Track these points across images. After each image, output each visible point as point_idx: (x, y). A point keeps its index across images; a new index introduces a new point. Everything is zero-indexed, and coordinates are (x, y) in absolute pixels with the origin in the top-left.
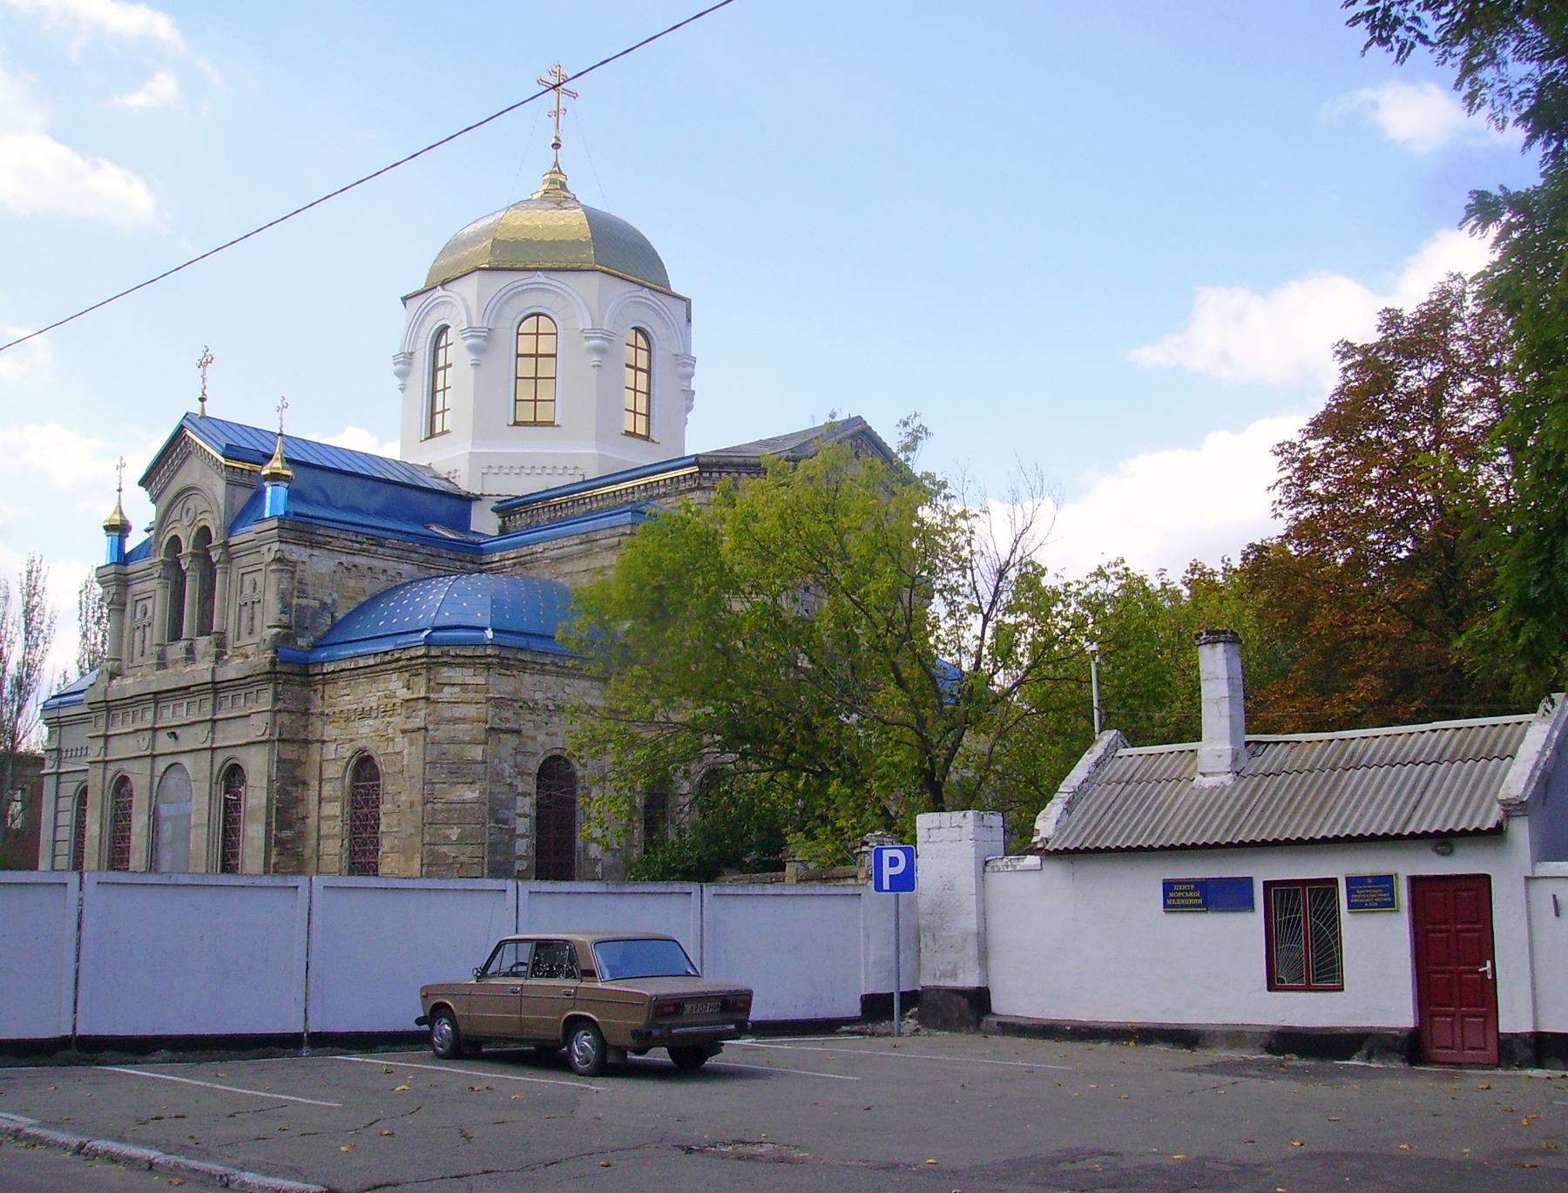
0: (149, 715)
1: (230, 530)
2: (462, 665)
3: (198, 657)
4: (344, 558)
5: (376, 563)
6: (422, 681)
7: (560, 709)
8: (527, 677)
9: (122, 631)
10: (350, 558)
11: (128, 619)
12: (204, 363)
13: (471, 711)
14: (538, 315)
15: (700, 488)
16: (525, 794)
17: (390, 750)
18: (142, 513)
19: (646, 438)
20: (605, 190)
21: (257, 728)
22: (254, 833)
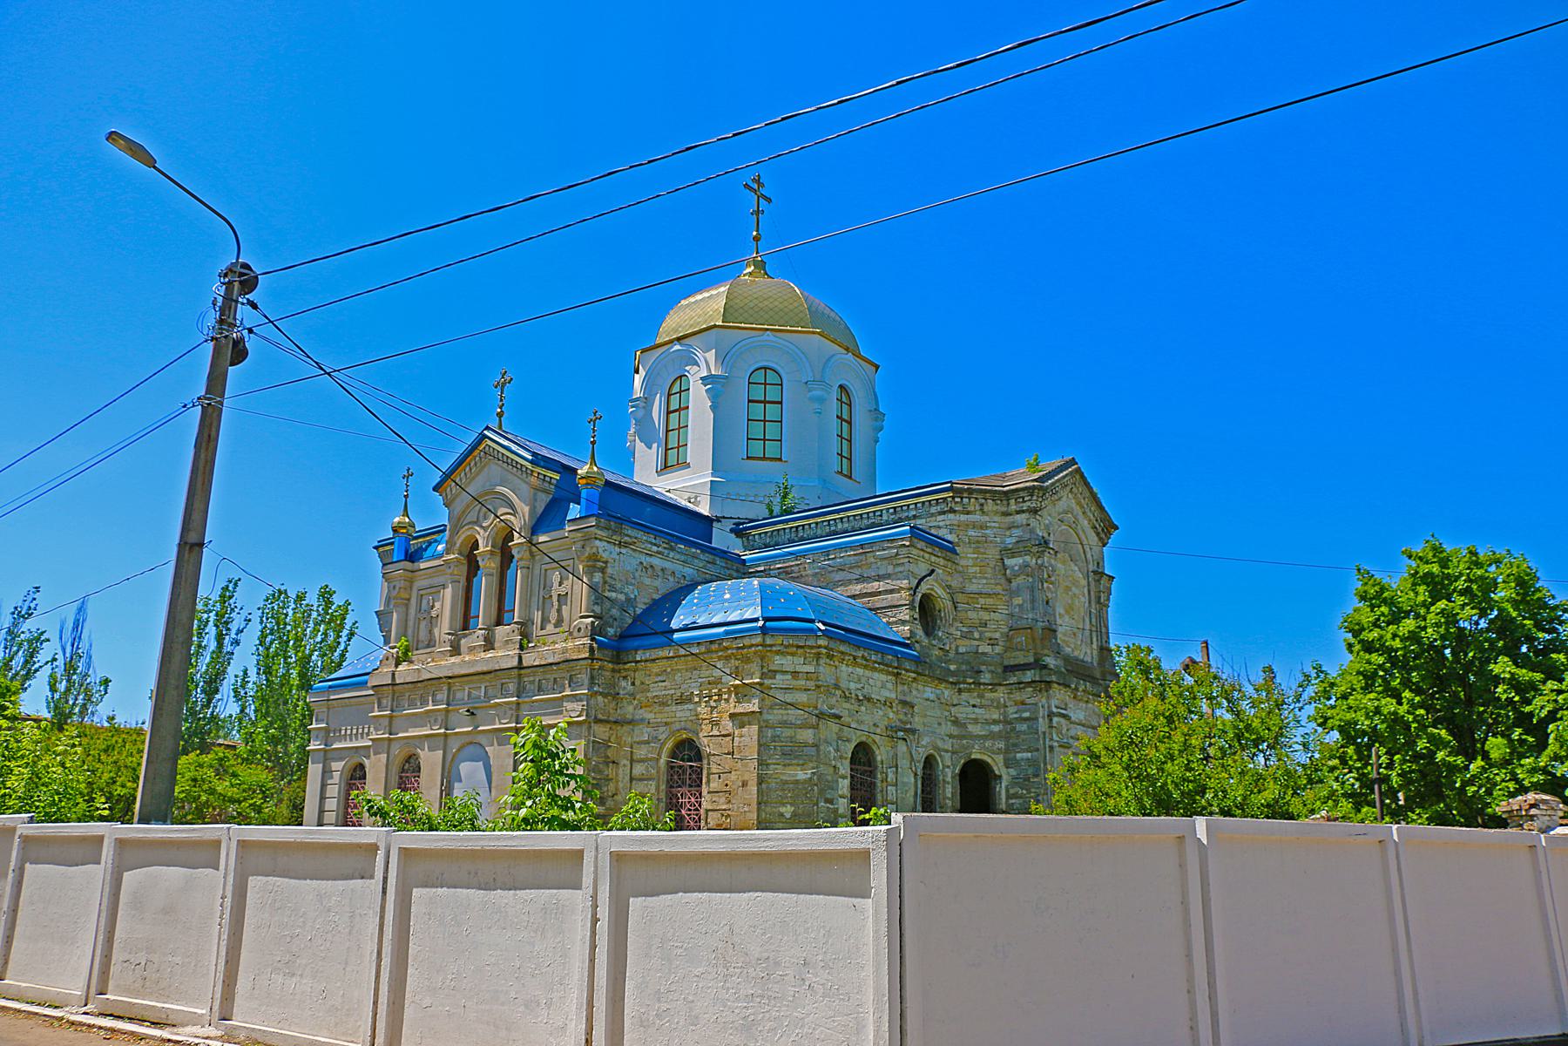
1: (535, 529)
5: (667, 565)
6: (754, 667)
7: (869, 699)
11: (412, 611)
14: (765, 368)
15: (952, 511)
16: (844, 777)
17: (715, 732)
22: (331, 804)
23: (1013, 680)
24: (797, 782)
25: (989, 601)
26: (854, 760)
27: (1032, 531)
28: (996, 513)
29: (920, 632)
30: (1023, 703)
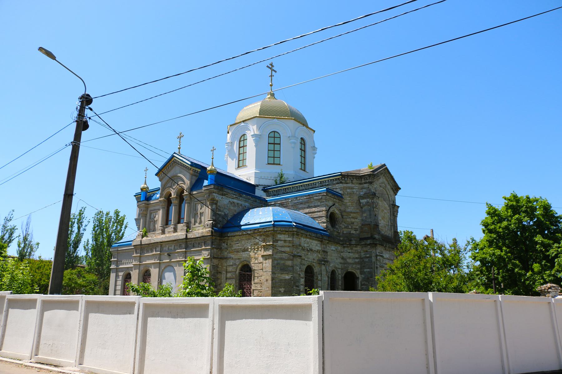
2: (284, 234)
3: (178, 231)
4: (231, 200)
5: (239, 202)
6: (270, 239)
7: (311, 250)
8: (302, 239)
9: (146, 222)
10: (233, 200)
11: (148, 218)
12: (180, 138)
13: (287, 249)
14: (274, 132)
15: (341, 183)
16: (302, 278)
17: (256, 262)
18: (155, 183)
19: (305, 171)
20: (284, 101)
21: (206, 254)
23: (363, 243)
24: (286, 279)
25: (355, 215)
26: (306, 272)
27: (370, 190)
28: (357, 183)
29: (330, 226)
30: (367, 251)
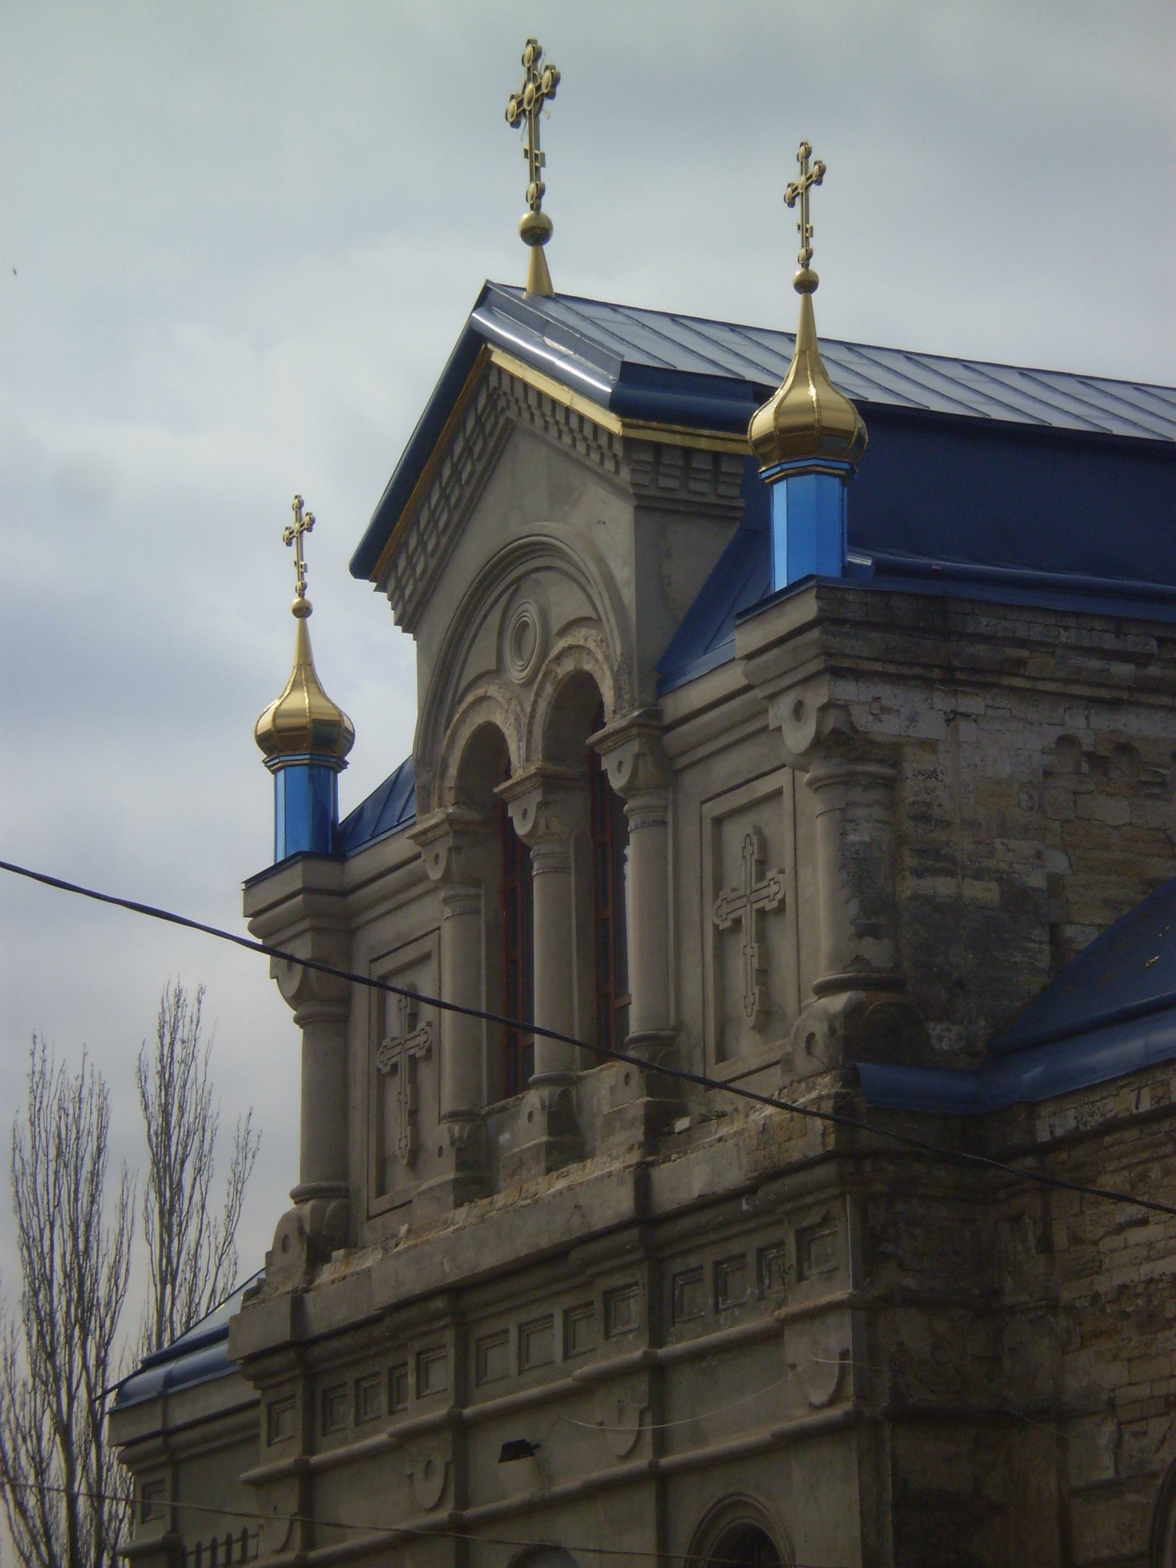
0: (442, 1374)
1: (664, 672)
4: (1077, 723)
21: (811, 1377)
